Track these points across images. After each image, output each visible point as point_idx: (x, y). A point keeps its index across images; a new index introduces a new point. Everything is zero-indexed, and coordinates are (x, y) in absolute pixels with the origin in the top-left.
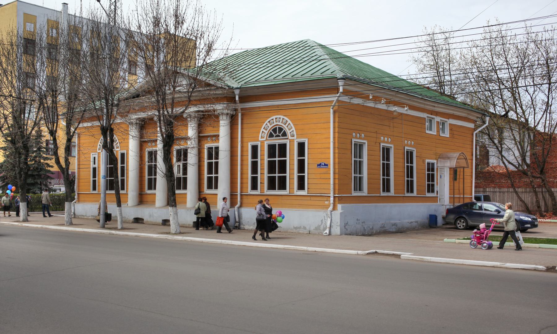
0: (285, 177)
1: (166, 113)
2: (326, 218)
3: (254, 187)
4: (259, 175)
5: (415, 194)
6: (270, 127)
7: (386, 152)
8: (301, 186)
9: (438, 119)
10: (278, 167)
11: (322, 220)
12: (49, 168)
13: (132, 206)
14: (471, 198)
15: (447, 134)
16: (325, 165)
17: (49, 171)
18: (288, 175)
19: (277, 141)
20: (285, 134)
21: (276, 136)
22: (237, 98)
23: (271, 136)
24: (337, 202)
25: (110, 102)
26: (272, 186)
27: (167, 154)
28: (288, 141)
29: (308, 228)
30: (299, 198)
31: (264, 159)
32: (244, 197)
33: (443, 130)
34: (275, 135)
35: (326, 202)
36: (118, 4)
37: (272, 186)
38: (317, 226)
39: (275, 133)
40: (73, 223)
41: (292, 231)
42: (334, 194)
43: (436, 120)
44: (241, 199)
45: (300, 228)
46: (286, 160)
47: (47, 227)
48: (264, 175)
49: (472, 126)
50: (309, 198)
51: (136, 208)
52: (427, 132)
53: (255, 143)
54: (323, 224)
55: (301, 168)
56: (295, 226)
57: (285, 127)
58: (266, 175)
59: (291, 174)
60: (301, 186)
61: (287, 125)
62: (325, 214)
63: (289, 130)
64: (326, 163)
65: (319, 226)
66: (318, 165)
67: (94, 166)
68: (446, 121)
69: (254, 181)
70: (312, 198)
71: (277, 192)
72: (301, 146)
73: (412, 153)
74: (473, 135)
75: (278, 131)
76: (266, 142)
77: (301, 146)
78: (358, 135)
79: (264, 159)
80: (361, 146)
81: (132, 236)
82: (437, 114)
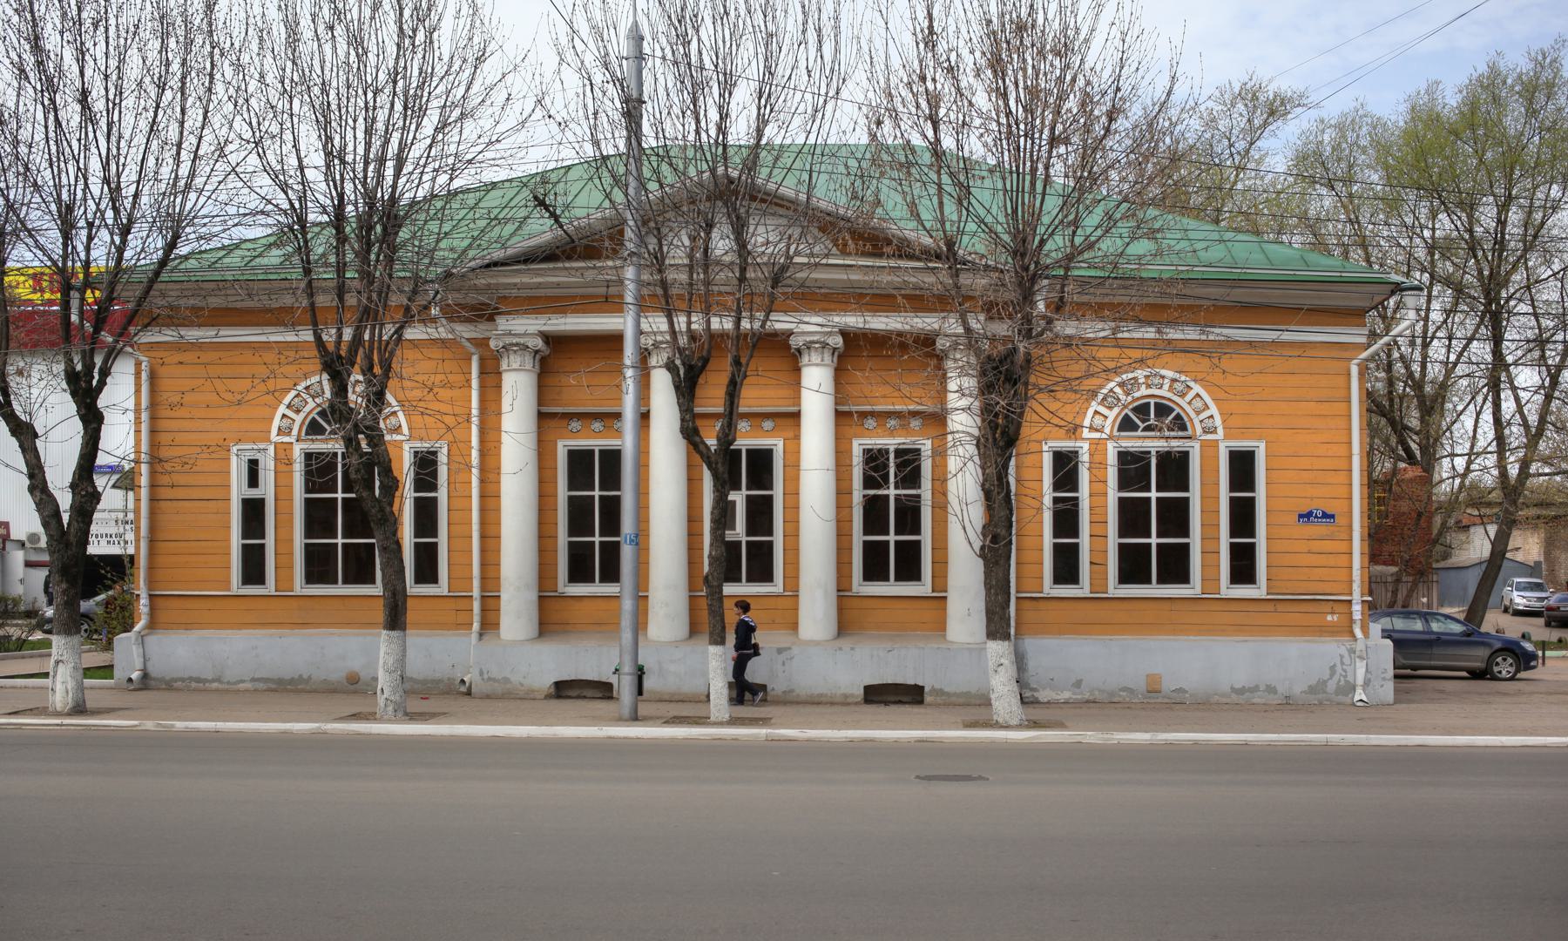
2: (1347, 660)
4: (1084, 540)
6: (1164, 392)
8: (1243, 570)
11: (1333, 668)
16: (1325, 515)
19: (1153, 444)
20: (1180, 424)
21: (1145, 429)
23: (1126, 425)
25: (350, 256)
28: (1197, 446)
29: (1280, 689)
30: (1234, 607)
34: (1142, 426)
35: (1329, 618)
38: (1313, 682)
40: (90, 704)
41: (1225, 700)
45: (1255, 689)
47: (221, 725)
50: (1270, 607)
53: (1065, 445)
54: (1336, 678)
56: (1238, 686)
57: (1184, 405)
59: (1210, 537)
60: (1243, 570)
61: (1188, 398)
62: (1343, 650)
63: (1198, 413)
64: (1329, 512)
65: (1323, 683)
66: (1301, 516)
67: (254, 493)
70: (1280, 607)
71: (1154, 590)
72: (1242, 466)
75: (1139, 416)
76: (1110, 446)
77: (1242, 466)
79: (1099, 496)
81: (881, 741)
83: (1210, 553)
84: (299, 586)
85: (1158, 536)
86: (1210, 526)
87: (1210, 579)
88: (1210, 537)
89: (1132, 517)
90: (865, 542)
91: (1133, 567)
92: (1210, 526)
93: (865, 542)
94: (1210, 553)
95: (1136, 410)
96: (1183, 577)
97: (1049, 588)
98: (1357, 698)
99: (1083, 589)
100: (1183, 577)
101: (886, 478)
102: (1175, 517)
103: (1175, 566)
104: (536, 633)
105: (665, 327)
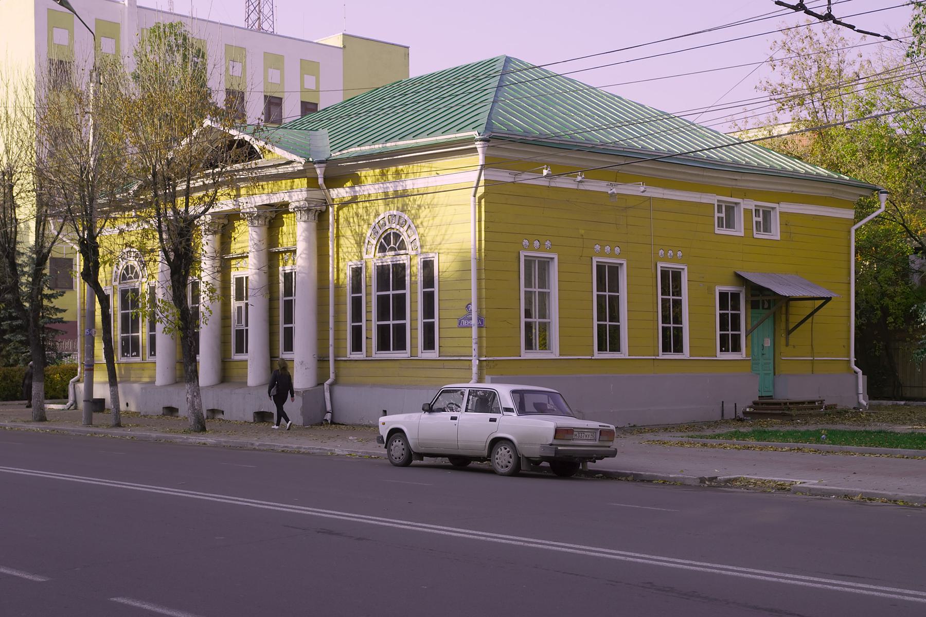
0: (404, 325)
1: (170, 212)
3: (357, 347)
4: (364, 324)
5: (686, 354)
7: (608, 277)
8: (429, 344)
9: (751, 204)
10: (393, 307)
12: (59, 315)
13: (212, 386)
14: (849, 361)
15: (776, 233)
17: (60, 321)
18: (407, 322)
19: (389, 259)
20: (402, 246)
22: (321, 181)
24: (485, 372)
26: (383, 345)
27: (178, 288)
31: (370, 294)
32: (342, 364)
33: (766, 226)
36: (266, 10)
37: (383, 345)
39: (389, 244)
42: (480, 355)
43: (742, 207)
44: (337, 369)
46: (405, 294)
48: (371, 324)
49: (850, 214)
51: (171, 389)
52: (718, 231)
55: (429, 311)
58: (374, 324)
60: (429, 344)
68: (773, 208)
69: (357, 332)
73: (677, 275)
74: (850, 232)
78: (537, 244)
80: (544, 265)
82: (745, 194)
96: (403, 348)
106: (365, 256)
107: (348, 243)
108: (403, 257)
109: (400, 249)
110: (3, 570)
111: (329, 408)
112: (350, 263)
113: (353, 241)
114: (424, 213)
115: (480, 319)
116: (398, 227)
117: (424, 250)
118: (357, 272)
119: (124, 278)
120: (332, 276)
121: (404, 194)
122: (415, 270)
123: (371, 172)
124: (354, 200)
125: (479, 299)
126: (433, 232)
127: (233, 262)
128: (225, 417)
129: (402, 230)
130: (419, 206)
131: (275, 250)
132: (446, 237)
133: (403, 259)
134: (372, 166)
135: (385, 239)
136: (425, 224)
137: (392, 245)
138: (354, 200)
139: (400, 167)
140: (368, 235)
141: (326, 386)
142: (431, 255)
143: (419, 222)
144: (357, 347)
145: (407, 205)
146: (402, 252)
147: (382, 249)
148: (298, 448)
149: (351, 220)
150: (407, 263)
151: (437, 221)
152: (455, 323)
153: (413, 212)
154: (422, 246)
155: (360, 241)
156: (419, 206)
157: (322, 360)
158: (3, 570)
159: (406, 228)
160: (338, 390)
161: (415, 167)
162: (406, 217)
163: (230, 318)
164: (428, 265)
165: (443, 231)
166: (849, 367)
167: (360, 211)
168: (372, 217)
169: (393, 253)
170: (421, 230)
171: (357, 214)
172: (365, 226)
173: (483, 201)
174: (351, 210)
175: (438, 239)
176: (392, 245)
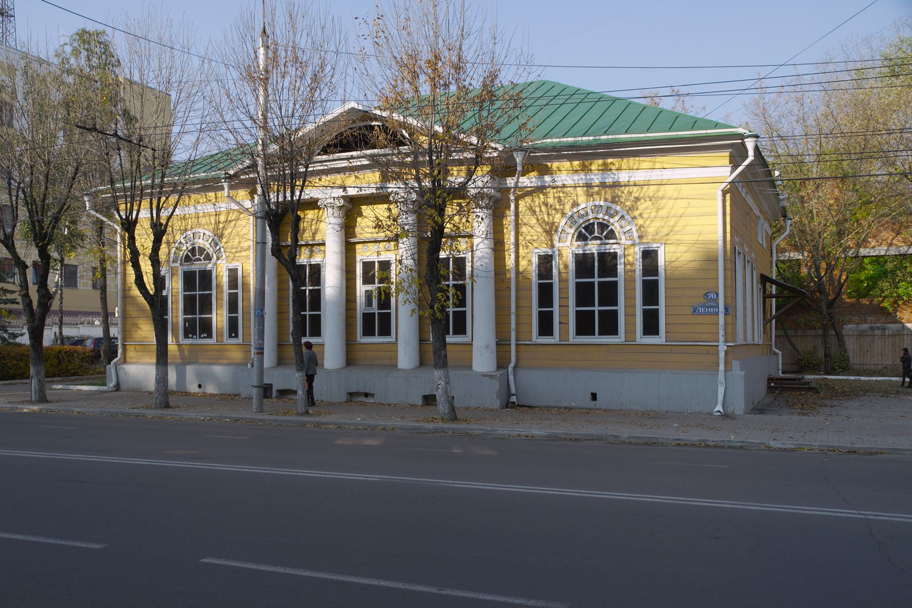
3: (546, 327)
4: (556, 309)
14: (771, 346)
20: (611, 235)
32: (523, 348)
42: (726, 341)
71: (597, 339)
83: (630, 315)
84: (573, 338)
85: (599, 306)
86: (630, 298)
87: (630, 331)
88: (630, 306)
89: (584, 294)
90: (617, 305)
91: (584, 325)
92: (630, 298)
93: (617, 305)
94: (630, 315)
95: (586, 228)
96: (614, 331)
97: (536, 338)
98: (716, 409)
99: (555, 339)
100: (614, 331)
101: (457, 280)
102: (609, 293)
103: (609, 325)
104: (417, 363)
105: (64, 329)
106: (557, 244)
107: (532, 230)
108: (615, 246)
109: (607, 237)
110: (2, 535)
111: (513, 391)
112: (537, 251)
113: (540, 230)
114: (642, 205)
115: (726, 309)
116: (606, 217)
117: (644, 241)
118: (546, 262)
119: (187, 259)
120: (510, 261)
121: (616, 185)
122: (629, 256)
123: (566, 164)
124: (541, 189)
125: (725, 287)
126: (657, 224)
127: (358, 247)
128: (378, 399)
129: (612, 220)
130: (637, 199)
131: (353, 240)
132: (676, 229)
133: (612, 247)
134: (571, 158)
135: (586, 228)
136: (645, 216)
137: (596, 234)
138: (541, 189)
139: (610, 161)
140: (562, 224)
141: (510, 369)
142: (655, 245)
143: (636, 213)
144: (546, 327)
145: (619, 197)
146: (611, 241)
147: (581, 237)
148: (492, 430)
149: (537, 209)
150: (619, 252)
151: (662, 213)
152: (689, 310)
153: (628, 203)
154: (640, 237)
155: (550, 230)
156: (637, 199)
157: (502, 343)
158: (2, 535)
159: (617, 218)
160: (523, 374)
161: (625, 162)
162: (618, 208)
163: (355, 301)
164: (649, 256)
165: (672, 223)
166: (771, 349)
167: (551, 201)
168: (568, 207)
169: (598, 242)
170: (640, 222)
171: (546, 204)
172: (558, 216)
173: (728, 196)
174: (537, 200)
175: (665, 231)
176: (596, 234)
